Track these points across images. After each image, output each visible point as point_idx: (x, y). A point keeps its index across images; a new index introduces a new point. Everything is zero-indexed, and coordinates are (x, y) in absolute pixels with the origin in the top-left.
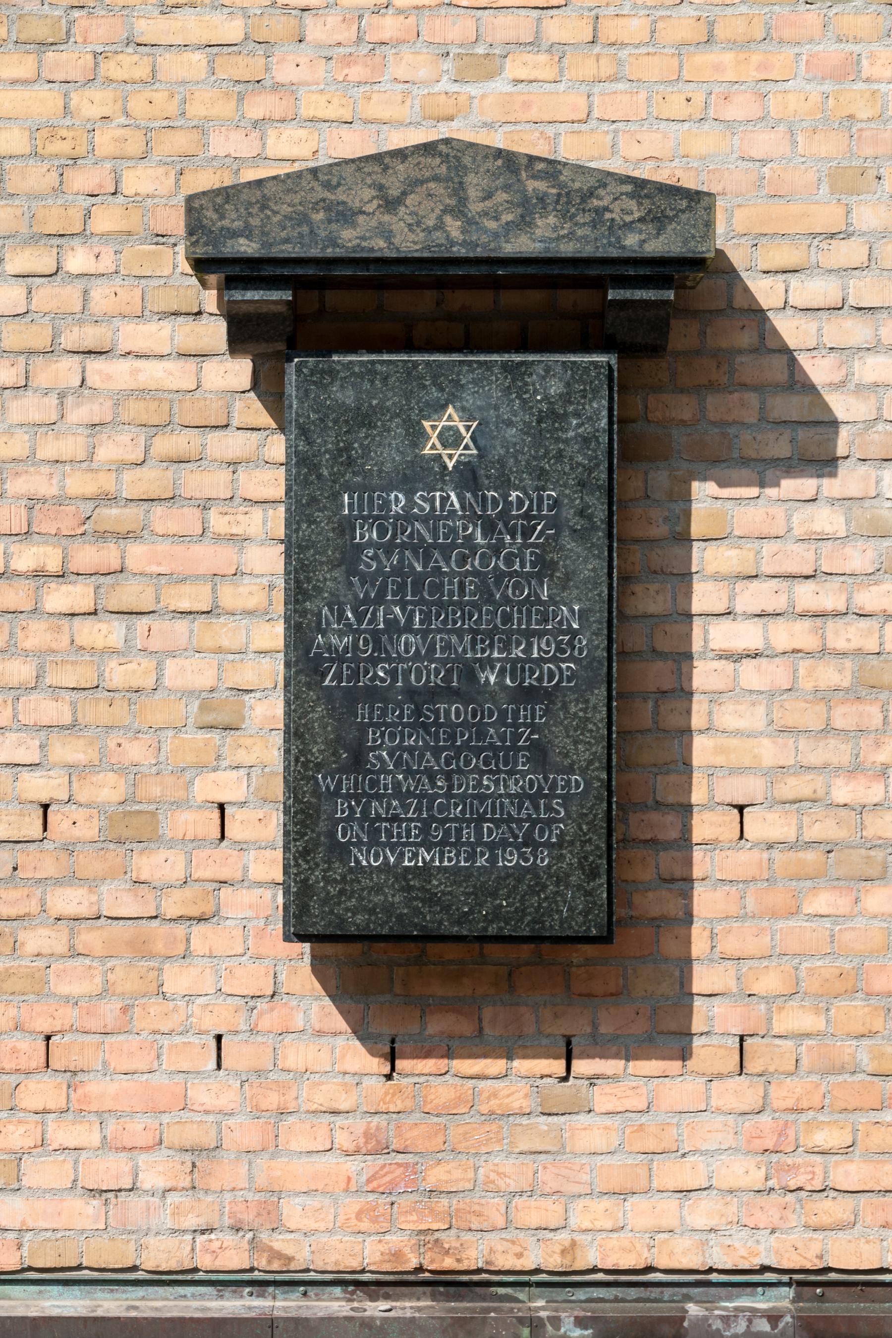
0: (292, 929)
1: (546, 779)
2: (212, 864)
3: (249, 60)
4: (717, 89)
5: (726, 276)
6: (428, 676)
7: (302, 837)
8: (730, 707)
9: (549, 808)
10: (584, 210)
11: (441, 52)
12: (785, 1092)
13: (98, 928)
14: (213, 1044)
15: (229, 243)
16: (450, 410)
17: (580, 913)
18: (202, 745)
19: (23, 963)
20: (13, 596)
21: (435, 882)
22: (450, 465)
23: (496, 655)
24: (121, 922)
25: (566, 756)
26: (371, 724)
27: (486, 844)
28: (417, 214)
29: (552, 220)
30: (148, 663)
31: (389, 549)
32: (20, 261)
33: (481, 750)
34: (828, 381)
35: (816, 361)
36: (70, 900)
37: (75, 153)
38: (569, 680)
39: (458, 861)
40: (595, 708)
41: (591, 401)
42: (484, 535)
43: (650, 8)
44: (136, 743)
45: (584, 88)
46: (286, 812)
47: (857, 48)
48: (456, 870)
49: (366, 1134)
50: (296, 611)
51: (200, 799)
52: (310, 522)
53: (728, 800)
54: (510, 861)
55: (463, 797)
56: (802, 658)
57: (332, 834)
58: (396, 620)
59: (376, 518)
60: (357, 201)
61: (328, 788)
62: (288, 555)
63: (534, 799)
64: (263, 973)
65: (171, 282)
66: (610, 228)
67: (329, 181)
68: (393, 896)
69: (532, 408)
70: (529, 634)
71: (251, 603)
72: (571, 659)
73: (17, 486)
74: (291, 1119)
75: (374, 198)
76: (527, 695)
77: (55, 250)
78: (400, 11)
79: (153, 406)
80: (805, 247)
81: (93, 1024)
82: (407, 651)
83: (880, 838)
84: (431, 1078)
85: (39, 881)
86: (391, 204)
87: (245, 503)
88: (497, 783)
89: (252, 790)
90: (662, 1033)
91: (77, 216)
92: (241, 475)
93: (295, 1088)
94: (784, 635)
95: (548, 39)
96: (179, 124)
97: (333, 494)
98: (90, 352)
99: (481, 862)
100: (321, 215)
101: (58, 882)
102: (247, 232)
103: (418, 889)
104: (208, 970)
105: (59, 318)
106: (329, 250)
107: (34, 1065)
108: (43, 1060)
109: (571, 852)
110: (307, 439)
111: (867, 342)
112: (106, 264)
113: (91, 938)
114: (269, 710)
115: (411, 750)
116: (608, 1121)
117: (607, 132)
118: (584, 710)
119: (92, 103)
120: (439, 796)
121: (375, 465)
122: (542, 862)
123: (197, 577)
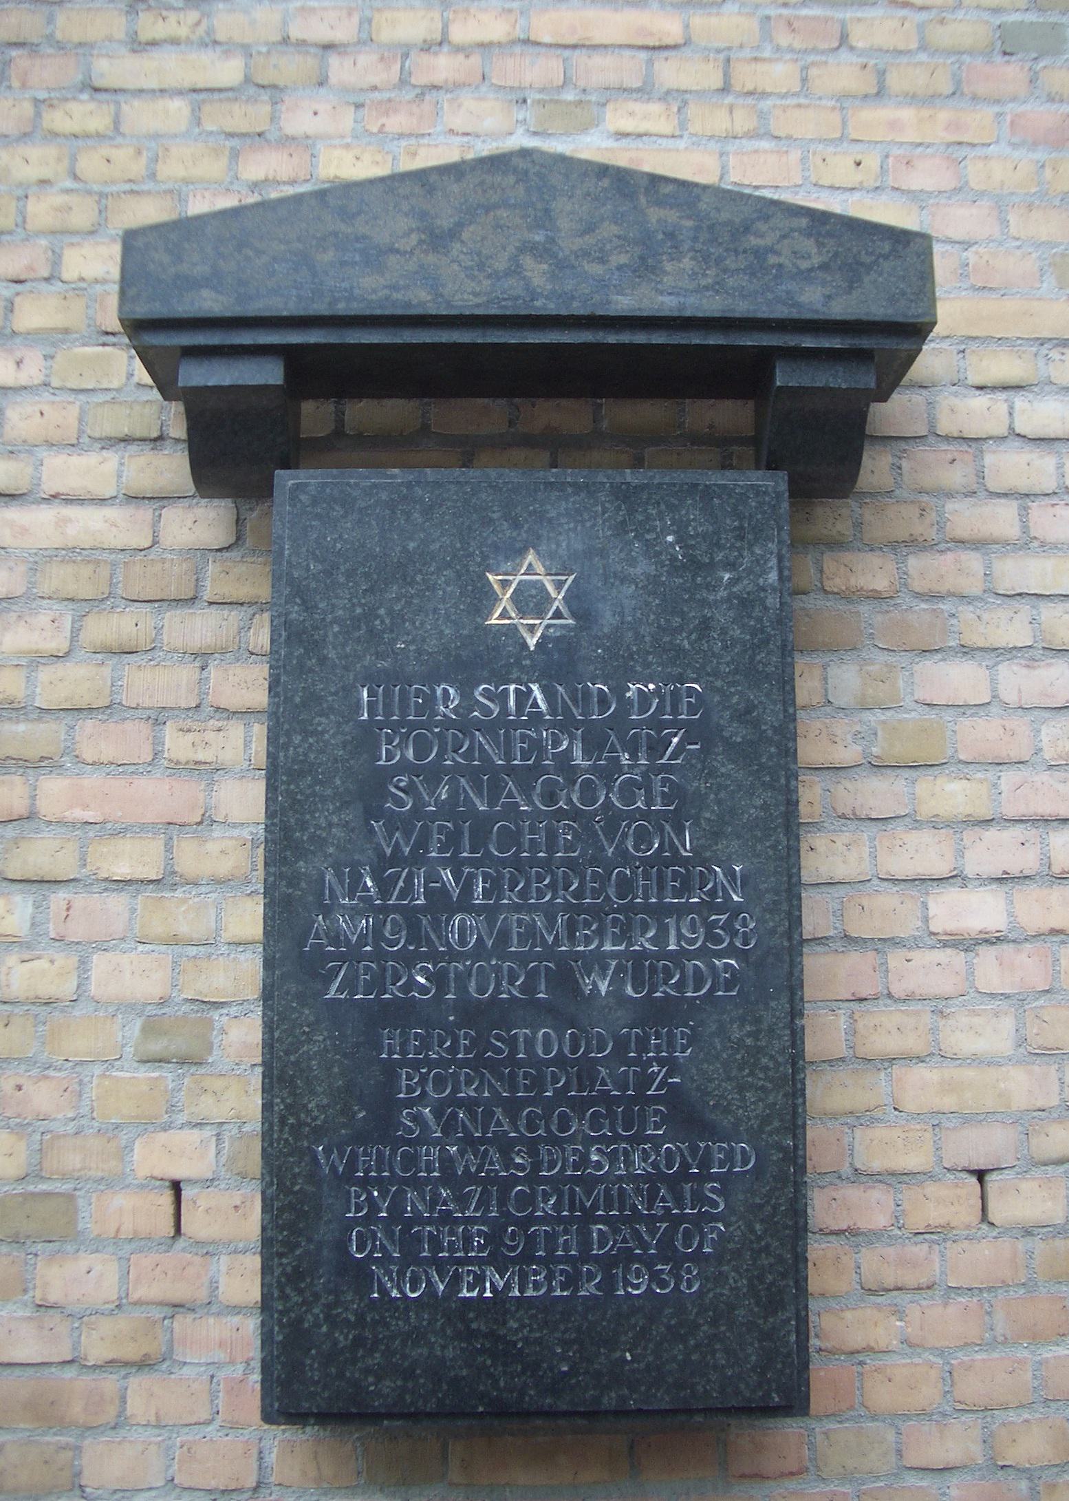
0: (276, 1405)
1: (694, 1149)
2: (157, 1279)
4: (896, 151)
5: (924, 392)
6: (498, 984)
7: (292, 1250)
9: (699, 1198)
10: (736, 251)
11: (514, 97)
16: (531, 557)
17: (754, 1369)
18: (145, 1088)
21: (513, 1324)
22: (532, 642)
23: (608, 947)
24: (18, 1371)
25: (726, 1110)
28: (479, 254)
29: (687, 263)
31: (434, 775)
38: (729, 986)
39: (551, 1289)
40: (771, 1030)
41: (751, 545)
42: (587, 753)
48: (547, 1304)
51: (143, 1172)
52: (306, 733)
53: (964, 1163)
54: (637, 1287)
55: (560, 1180)
57: (342, 1246)
58: (444, 890)
59: (412, 726)
61: (333, 1168)
63: (674, 1183)
68: (443, 1347)
70: (660, 912)
71: (224, 867)
72: (731, 951)
75: (411, 230)
76: (658, 1014)
78: (459, 49)
79: (86, 571)
82: (463, 941)
86: (437, 240)
87: (217, 715)
88: (613, 1157)
89: (223, 1160)
92: (213, 672)
96: (145, 187)
97: (343, 688)
99: (588, 1289)
100: (329, 256)
103: (485, 1336)
104: (153, 1448)
109: (736, 1269)
110: (304, 602)
112: (32, 371)
114: (243, 1035)
115: (469, 1105)
118: (755, 1035)
120: (517, 1180)
121: (413, 641)
122: (689, 1287)
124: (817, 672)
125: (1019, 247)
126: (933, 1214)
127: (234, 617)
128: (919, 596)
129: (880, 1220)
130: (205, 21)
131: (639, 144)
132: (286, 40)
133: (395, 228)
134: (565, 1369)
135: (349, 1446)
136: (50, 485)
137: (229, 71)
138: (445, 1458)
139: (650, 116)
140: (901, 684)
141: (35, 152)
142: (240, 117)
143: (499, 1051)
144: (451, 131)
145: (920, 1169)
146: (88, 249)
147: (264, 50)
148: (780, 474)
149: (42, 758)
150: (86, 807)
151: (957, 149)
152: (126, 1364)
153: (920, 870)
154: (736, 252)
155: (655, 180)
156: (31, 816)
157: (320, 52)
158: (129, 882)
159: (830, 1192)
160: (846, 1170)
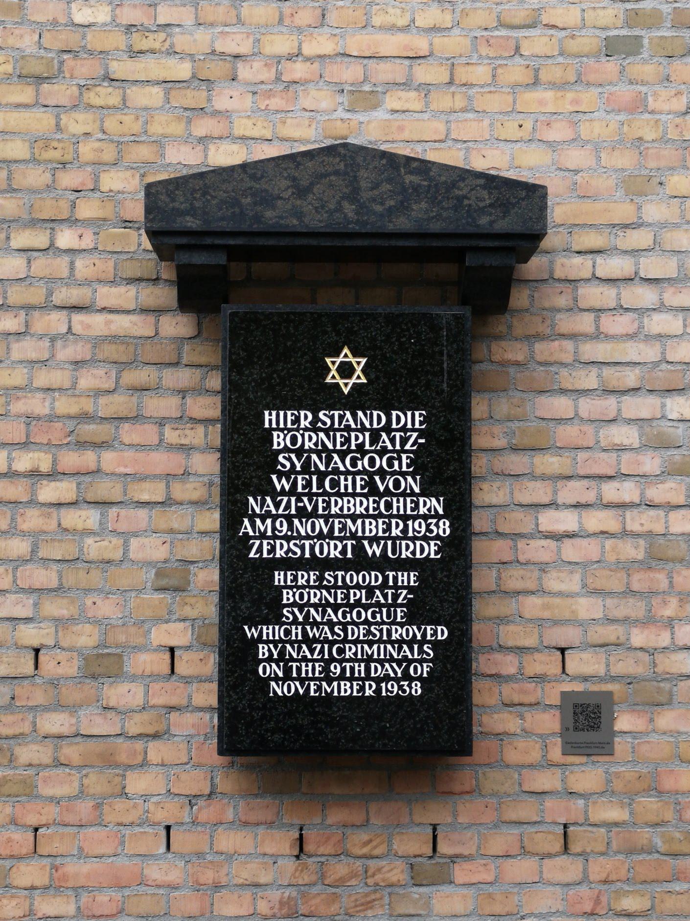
0: (225, 746)
2: (162, 694)
3: (196, 93)
4: (542, 118)
5: (548, 255)
11: (337, 89)
12: (598, 868)
13: (76, 744)
14: (164, 833)
15: (179, 220)
18: (157, 602)
19: (17, 772)
20: (15, 491)
24: (94, 739)
25: (435, 611)
27: (373, 679)
28: (321, 200)
29: (424, 205)
30: (117, 541)
32: (22, 239)
33: (370, 606)
34: (624, 333)
35: (615, 318)
36: (56, 723)
37: (64, 159)
43: (492, 58)
44: (107, 601)
45: (443, 117)
46: (221, 654)
47: (644, 89)
49: (281, 903)
50: (228, 500)
53: (554, 644)
59: (290, 430)
60: (276, 188)
62: (223, 459)
64: (202, 778)
66: (468, 211)
67: (255, 173)
69: (407, 348)
71: (195, 496)
73: (18, 407)
74: (224, 891)
75: (289, 187)
77: (48, 231)
78: (308, 59)
79: (122, 348)
81: (70, 818)
84: (330, 858)
86: (302, 192)
89: (195, 637)
91: (64, 205)
92: (189, 400)
94: (596, 520)
95: (416, 81)
96: (142, 139)
98: (74, 307)
99: (368, 692)
100: (249, 200)
101: (46, 709)
102: (192, 211)
104: (160, 776)
106: (255, 226)
107: (24, 851)
111: (653, 304)
112: (88, 242)
113: (71, 752)
116: (465, 891)
117: (460, 149)
118: (448, 577)
119: (78, 123)
123: (155, 476)
124: (486, 402)
126: (539, 669)
127: (198, 372)
128: (540, 364)
129: (512, 670)
130: (169, 39)
131: (403, 116)
132: (213, 52)
133: (280, 185)
135: (254, 776)
136: (101, 303)
137: (183, 70)
138: (301, 781)
140: (528, 408)
141: (81, 116)
142: (193, 97)
143: (329, 582)
144: (305, 110)
145: (532, 646)
147: (202, 58)
148: (468, 307)
149: (103, 443)
150: (126, 466)
152: (147, 735)
154: (448, 199)
155: (409, 159)
156: (98, 471)
158: (148, 503)
159: (486, 656)
160: (495, 645)
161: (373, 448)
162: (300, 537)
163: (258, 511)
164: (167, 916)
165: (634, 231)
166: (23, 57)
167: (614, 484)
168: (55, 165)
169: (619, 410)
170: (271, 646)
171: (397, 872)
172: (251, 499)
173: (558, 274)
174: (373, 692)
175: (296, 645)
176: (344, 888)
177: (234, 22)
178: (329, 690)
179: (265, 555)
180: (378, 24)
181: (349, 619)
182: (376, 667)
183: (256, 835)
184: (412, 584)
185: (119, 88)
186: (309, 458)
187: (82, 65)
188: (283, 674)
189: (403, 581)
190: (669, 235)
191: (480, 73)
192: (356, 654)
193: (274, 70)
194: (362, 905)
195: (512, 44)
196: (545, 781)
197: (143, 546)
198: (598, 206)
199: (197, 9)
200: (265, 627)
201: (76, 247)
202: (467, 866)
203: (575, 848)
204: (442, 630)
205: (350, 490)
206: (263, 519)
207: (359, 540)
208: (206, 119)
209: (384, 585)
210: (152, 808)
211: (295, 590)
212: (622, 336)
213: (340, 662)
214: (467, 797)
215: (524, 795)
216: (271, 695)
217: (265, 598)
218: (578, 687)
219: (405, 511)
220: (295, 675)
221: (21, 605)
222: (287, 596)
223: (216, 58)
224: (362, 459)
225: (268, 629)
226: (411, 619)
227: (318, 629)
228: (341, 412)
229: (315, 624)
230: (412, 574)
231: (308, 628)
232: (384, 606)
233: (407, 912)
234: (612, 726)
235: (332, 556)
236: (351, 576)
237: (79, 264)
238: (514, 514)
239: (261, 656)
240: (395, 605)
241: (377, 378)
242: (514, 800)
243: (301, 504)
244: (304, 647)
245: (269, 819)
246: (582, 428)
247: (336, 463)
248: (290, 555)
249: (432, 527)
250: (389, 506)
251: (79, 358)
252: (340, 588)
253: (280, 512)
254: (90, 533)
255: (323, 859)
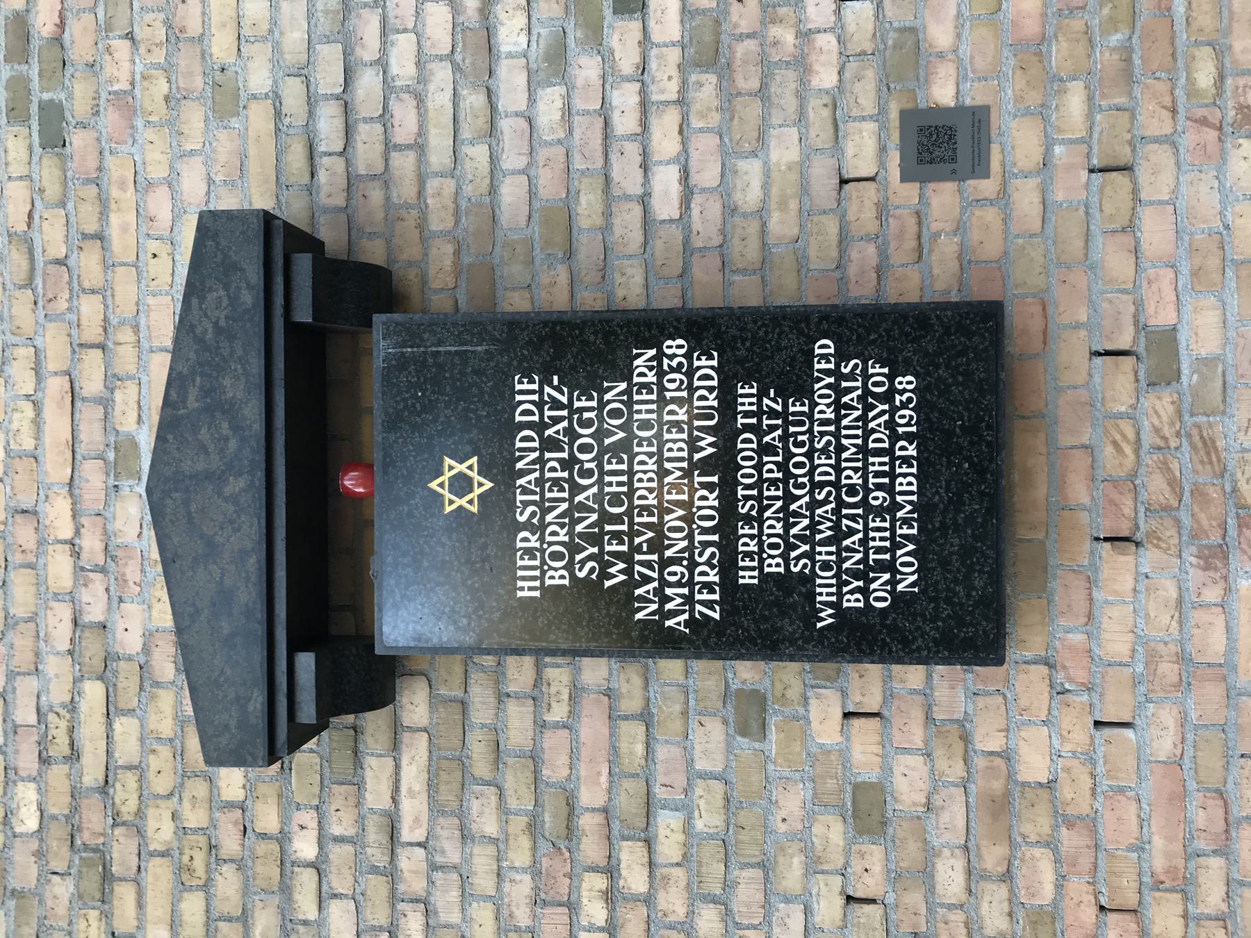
4: (144, 229)
5: (317, 215)
8: (738, 197)
12: (1154, 122)
13: (979, 849)
14: (1107, 732)
17: (970, 340)
18: (782, 735)
25: (793, 359)
26: (761, 568)
27: (892, 445)
29: (227, 382)
32: (306, 906)
33: (786, 449)
34: (415, 111)
36: (950, 877)
37: (205, 848)
44: (781, 803)
47: (104, 95)
51: (839, 739)
53: (834, 194)
56: (688, 125)
59: (543, 562)
65: (326, 755)
68: (952, 545)
69: (430, 401)
71: (637, 681)
73: (523, 917)
77: (296, 869)
78: (77, 532)
79: (444, 776)
80: (289, 140)
81: (1085, 862)
83: (874, 35)
84: (1140, 499)
85: (930, 910)
90: (1086, 255)
91: (262, 848)
93: (1152, 644)
94: (665, 141)
99: (912, 451)
101: (931, 889)
103: (944, 518)
105: (360, 867)
108: (1128, 917)
112: (309, 818)
113: (992, 857)
116: (1187, 310)
118: (744, 340)
119: (161, 830)
124: (509, 294)
125: (210, 144)
126: (870, 213)
127: (475, 676)
129: (871, 249)
130: (55, 709)
131: (145, 408)
132: (70, 652)
134: (967, 465)
136: (386, 803)
137: (94, 692)
138: (1030, 541)
139: (125, 398)
141: (151, 824)
143: (752, 507)
146: (222, 784)
149: (568, 804)
150: (599, 773)
151: (142, 185)
153: (639, 225)
157: (79, 629)
158: (648, 745)
159: (852, 286)
161: (566, 447)
162: (690, 548)
163: (654, 607)
164: (1226, 728)
165: (284, 102)
166: (80, 897)
167: (616, 117)
168: (213, 860)
169: (517, 114)
170: (845, 589)
171: (1161, 404)
172: (639, 616)
173: (340, 201)
174: (911, 444)
175: (844, 554)
176: (1184, 480)
177: (32, 625)
178: (909, 508)
179: (716, 597)
180: (33, 442)
181: (805, 480)
182: (875, 441)
183: (1106, 602)
184: (754, 391)
185: (116, 774)
186: (580, 535)
187: (90, 821)
188: (885, 572)
189: (750, 404)
190: (287, 57)
191: (90, 308)
192: (856, 470)
193: (91, 575)
194: (1208, 453)
195: (52, 269)
196: (1026, 199)
197: (705, 752)
198: (252, 152)
199: (19, 674)
200: (819, 599)
201: (316, 833)
202: (1150, 308)
203: (1124, 154)
204: (820, 347)
205: (624, 478)
206: (666, 599)
207: (693, 465)
208: (153, 663)
209: (756, 430)
210: (1068, 747)
211: (765, 556)
212: (420, 115)
213: (867, 491)
214: (1050, 310)
215: (1049, 230)
216: (916, 590)
217: (777, 597)
218: (894, 158)
219: (652, 402)
220: (887, 557)
221: (787, 920)
222: (774, 566)
223: (77, 648)
224: (582, 462)
225: (821, 594)
226: (804, 391)
227: (820, 523)
228: (518, 491)
229: (813, 527)
230: (740, 391)
231: (818, 537)
232: (786, 431)
233: (1219, 390)
234: (947, 110)
235: (716, 503)
236: (743, 476)
237: (337, 830)
238: (657, 253)
239: (861, 605)
240: (784, 414)
241: (470, 442)
242: (1055, 243)
243: (645, 545)
244: (846, 543)
245: (1084, 584)
246: (541, 164)
247: (587, 498)
248: (715, 562)
249: (674, 363)
250: (645, 425)
251: (457, 833)
252: (761, 492)
253: (655, 575)
254: (688, 828)
255: (1142, 510)
